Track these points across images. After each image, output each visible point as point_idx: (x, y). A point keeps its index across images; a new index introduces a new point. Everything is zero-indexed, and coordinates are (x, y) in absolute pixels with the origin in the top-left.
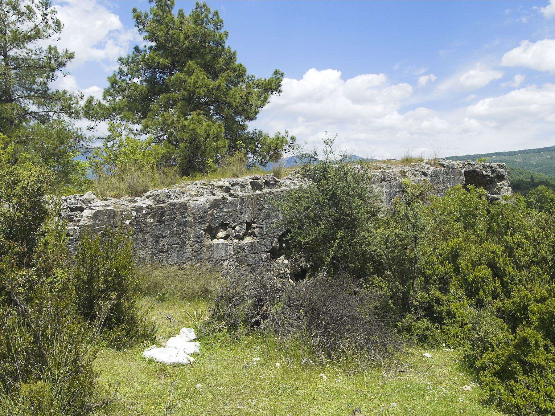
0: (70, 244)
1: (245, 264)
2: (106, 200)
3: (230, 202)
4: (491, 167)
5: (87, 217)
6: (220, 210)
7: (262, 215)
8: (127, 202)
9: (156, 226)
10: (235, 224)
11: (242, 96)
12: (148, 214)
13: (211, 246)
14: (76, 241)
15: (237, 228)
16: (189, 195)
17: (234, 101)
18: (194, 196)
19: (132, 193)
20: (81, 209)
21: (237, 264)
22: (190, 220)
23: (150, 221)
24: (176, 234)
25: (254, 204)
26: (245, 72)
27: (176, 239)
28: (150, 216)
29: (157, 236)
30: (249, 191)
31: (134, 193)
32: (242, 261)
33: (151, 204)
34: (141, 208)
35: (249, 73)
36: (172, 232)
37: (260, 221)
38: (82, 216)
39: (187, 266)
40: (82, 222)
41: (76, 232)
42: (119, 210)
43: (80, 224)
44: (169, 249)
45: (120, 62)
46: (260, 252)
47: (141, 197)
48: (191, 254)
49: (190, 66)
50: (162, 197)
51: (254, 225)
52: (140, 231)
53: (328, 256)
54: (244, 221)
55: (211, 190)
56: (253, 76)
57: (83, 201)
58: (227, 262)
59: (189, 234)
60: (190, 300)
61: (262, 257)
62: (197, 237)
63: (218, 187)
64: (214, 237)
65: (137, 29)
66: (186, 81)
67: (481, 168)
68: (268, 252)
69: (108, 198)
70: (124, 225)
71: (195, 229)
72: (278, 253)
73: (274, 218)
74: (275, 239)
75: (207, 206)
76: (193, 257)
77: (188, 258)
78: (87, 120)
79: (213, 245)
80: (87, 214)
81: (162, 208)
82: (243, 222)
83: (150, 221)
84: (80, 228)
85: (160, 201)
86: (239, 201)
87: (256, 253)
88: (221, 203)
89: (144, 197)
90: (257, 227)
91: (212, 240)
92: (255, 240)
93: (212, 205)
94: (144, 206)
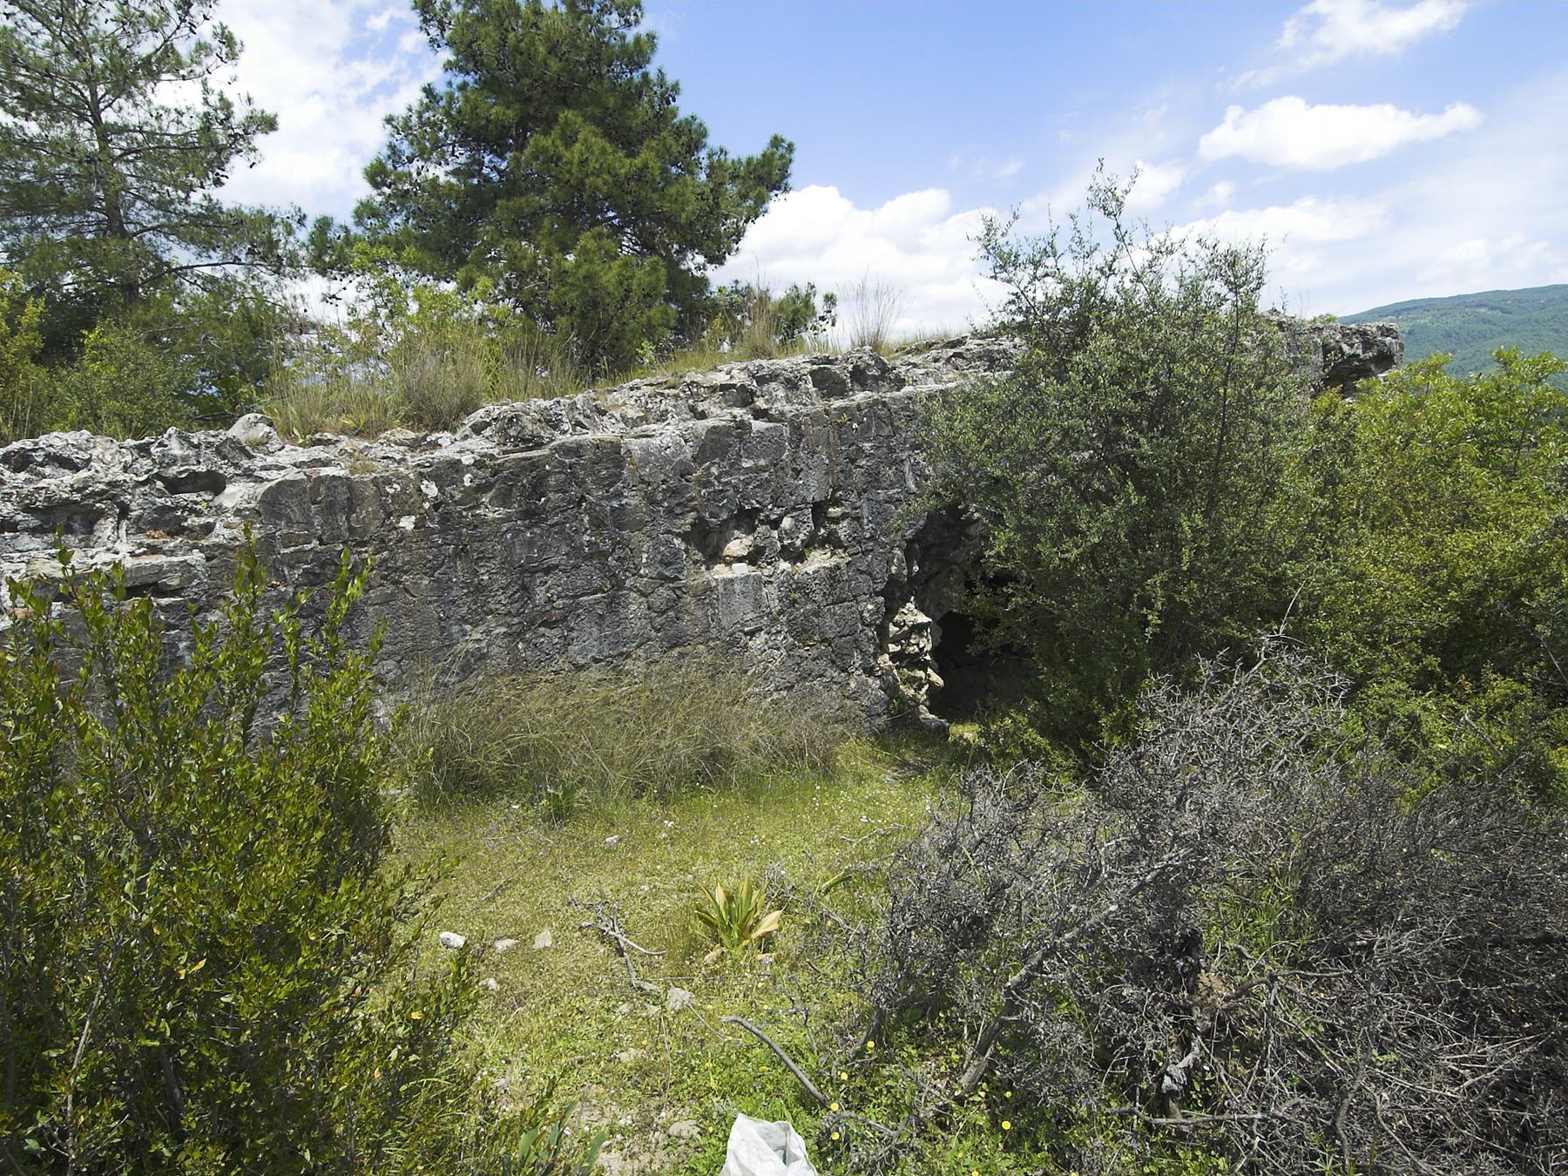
0: (174, 627)
1: (816, 638)
2: (319, 442)
3: (761, 434)
4: (1364, 333)
5: (238, 512)
6: (731, 465)
7: (858, 477)
8: (402, 448)
9: (517, 532)
10: (778, 511)
11: (703, 194)
12: (481, 489)
13: (709, 588)
14: (200, 610)
15: (787, 523)
16: (619, 418)
17: (683, 210)
18: (635, 423)
19: (421, 420)
20: (215, 484)
21: (791, 639)
22: (633, 502)
23: (492, 513)
24: (589, 557)
25: (831, 440)
26: (704, 135)
27: (590, 573)
28: (490, 494)
29: (523, 569)
30: (812, 402)
31: (427, 419)
32: (806, 631)
33: (491, 451)
34: (455, 466)
35: (713, 141)
36: (576, 551)
37: (853, 497)
38: (220, 510)
39: (636, 666)
40: (221, 534)
41: (196, 576)
42: (368, 477)
43: (212, 540)
44: (570, 610)
45: (389, 127)
46: (855, 597)
47: (454, 431)
48: (644, 622)
49: (567, 123)
50: (530, 427)
51: (834, 511)
52: (456, 555)
53: (1151, 607)
54: (804, 498)
55: (691, 401)
56: (721, 151)
57: (218, 452)
58: (763, 636)
59: (636, 552)
60: (663, 798)
61: (861, 613)
62: (661, 562)
63: (713, 389)
64: (714, 556)
65: (424, 37)
66: (560, 158)
67: (1338, 337)
68: (877, 594)
69: (330, 436)
70: (394, 535)
71: (654, 534)
72: (898, 594)
73: (892, 486)
74: (897, 551)
75: (688, 451)
76: (653, 633)
77: (636, 636)
78: (320, 277)
79: (714, 584)
80: (238, 499)
81: (533, 464)
82: (804, 501)
83: (492, 513)
84: (208, 559)
85: (524, 441)
86: (786, 431)
87: (845, 600)
88: (731, 440)
89: (467, 430)
90: (844, 516)
91: (708, 569)
92: (841, 558)
93: (703, 448)
94: (467, 459)
